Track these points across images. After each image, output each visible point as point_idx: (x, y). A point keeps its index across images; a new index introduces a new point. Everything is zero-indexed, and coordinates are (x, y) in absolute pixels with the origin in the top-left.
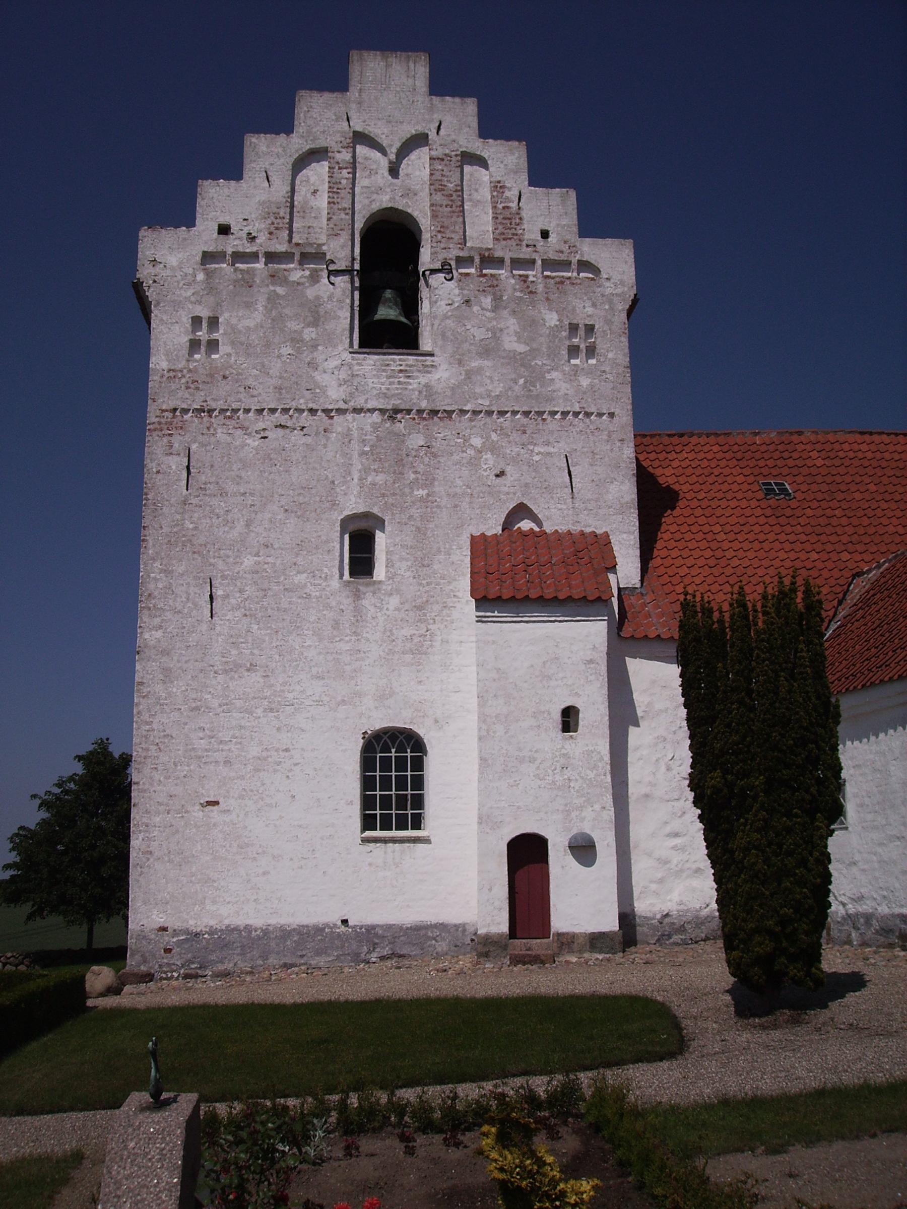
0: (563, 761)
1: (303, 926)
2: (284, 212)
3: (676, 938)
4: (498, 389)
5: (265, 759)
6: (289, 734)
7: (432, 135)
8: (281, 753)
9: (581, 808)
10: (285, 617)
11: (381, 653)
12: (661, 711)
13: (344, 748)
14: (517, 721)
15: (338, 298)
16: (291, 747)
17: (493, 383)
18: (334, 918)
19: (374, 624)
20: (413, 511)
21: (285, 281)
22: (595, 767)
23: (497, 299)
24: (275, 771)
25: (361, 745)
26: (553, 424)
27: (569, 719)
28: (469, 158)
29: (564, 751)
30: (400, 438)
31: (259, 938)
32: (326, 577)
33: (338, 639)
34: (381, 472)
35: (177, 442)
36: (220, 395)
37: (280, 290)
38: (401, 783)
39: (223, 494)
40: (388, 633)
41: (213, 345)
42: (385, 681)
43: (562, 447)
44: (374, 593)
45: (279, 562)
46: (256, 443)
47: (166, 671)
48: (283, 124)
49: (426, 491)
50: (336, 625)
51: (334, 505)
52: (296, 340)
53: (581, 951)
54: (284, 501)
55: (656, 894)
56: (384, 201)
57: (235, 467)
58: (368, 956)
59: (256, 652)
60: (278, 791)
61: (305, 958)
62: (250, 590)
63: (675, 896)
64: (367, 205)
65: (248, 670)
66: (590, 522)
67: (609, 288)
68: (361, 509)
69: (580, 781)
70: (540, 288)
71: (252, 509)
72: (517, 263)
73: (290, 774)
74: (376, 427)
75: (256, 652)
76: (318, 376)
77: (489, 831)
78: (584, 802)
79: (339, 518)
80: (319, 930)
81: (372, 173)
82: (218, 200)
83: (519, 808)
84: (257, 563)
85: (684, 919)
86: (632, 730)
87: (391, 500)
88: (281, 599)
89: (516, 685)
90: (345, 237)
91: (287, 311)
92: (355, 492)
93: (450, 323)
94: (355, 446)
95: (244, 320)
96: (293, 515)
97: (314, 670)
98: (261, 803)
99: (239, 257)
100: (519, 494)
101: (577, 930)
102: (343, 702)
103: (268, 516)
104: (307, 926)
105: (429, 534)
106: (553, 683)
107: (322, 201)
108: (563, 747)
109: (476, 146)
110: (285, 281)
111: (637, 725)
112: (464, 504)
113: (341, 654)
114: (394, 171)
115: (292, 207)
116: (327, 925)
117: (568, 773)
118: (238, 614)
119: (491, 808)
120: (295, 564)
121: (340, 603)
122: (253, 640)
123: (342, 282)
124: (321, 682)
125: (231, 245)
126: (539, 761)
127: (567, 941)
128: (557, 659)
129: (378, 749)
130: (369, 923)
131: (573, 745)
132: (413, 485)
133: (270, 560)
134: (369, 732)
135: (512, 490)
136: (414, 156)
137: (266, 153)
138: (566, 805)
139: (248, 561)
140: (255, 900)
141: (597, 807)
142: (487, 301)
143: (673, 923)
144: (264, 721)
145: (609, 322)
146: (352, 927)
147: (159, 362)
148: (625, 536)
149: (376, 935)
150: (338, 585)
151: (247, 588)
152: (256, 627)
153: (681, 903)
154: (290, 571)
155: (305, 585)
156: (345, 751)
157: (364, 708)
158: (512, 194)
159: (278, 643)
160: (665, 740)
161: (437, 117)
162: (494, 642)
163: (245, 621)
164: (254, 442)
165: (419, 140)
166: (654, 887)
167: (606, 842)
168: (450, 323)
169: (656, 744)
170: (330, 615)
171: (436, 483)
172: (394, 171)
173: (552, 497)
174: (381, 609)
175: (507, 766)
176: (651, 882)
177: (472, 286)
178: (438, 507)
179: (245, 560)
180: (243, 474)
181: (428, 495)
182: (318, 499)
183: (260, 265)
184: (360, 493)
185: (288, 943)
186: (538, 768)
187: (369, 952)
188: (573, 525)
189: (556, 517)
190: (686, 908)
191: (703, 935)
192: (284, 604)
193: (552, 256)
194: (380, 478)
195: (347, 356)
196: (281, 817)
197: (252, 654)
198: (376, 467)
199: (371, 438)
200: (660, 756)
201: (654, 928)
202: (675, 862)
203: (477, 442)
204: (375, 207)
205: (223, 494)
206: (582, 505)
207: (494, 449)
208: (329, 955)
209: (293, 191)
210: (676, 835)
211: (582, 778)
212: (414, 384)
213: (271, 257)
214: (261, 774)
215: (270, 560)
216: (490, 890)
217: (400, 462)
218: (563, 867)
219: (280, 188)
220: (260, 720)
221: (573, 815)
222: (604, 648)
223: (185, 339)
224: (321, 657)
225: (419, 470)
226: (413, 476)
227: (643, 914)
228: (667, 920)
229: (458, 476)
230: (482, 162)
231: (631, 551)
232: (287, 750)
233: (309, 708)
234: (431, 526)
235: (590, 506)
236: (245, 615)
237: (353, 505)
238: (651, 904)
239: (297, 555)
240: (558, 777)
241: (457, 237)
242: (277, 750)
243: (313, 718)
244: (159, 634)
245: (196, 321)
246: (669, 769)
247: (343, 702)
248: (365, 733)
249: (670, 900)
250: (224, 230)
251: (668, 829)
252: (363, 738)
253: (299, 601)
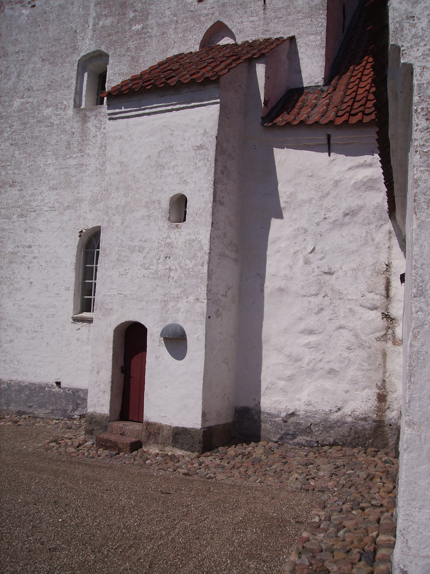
0: (167, 250)
1: (32, 384)
3: (300, 439)
5: (16, 253)
6: (32, 234)
8: (26, 249)
9: (177, 299)
10: (36, 143)
11: (98, 165)
12: (305, 202)
13: (66, 244)
14: (132, 211)
16: (32, 244)
18: (52, 380)
19: (94, 141)
22: (194, 257)
24: (22, 263)
25: (78, 242)
27: (179, 206)
29: (169, 241)
31: (6, 390)
32: (65, 108)
33: (68, 156)
34: (109, 16)
40: (104, 148)
42: (98, 188)
44: (96, 116)
45: (35, 101)
46: (28, 11)
49: (142, 25)
50: (69, 146)
51: (74, 49)
53: (164, 444)
54: (42, 52)
55: (284, 391)
57: (14, 33)
58: (73, 413)
59: (16, 171)
60: (22, 278)
61: (32, 409)
62: (16, 125)
63: (304, 396)
65: (10, 186)
66: (279, 29)
68: (93, 48)
69: (179, 271)
71: (23, 62)
73: (30, 266)
75: (16, 171)
77: (101, 317)
78: (181, 292)
79: (77, 60)
80: (41, 388)
83: (125, 296)
84: (22, 103)
85: (312, 421)
86: (275, 222)
87: (114, 38)
88: (35, 128)
89: (134, 177)
92: (89, 36)
96: (47, 62)
97: (52, 182)
98: (12, 287)
100: (217, 14)
101: (165, 422)
102: (68, 207)
103: (31, 66)
104: (34, 384)
105: (141, 60)
106: (165, 172)
108: (168, 237)
111: (280, 216)
112: (171, 30)
113: (70, 168)
116: (47, 385)
117: (170, 263)
118: (8, 144)
119: (105, 295)
120: (45, 100)
121: (72, 127)
122: (15, 163)
124: (55, 192)
126: (146, 250)
127: (154, 431)
128: (171, 147)
129: (96, 248)
130: (74, 387)
131: (177, 234)
132: (134, 20)
133: (30, 100)
134: (84, 231)
135: (211, 11)
138: (165, 295)
139: (17, 103)
140: (4, 361)
141: (191, 298)
143: (299, 424)
144: (17, 224)
146: (64, 389)
148: (312, 37)
149: (79, 396)
150: (72, 113)
151: (14, 124)
152: (17, 152)
153: (309, 404)
154: (42, 107)
155: (51, 116)
156: (67, 247)
157: (82, 211)
159: (30, 164)
160: (306, 231)
162: (121, 137)
163: (12, 148)
166: (282, 384)
167: (196, 336)
169: (296, 237)
170: (64, 137)
171: (150, 17)
173: (246, 12)
174: (100, 129)
175: (120, 256)
176: (279, 378)
178: (150, 37)
179: (15, 102)
180: (19, 37)
181: (143, 28)
182: (64, 46)
184: (92, 37)
185: (22, 396)
186: (145, 257)
187: (74, 410)
188: (263, 34)
190: (314, 410)
191: (331, 440)
192: (36, 134)
194: (108, 21)
196: (23, 299)
197: (14, 173)
198: (106, 13)
200: (298, 248)
201: (277, 425)
202: (306, 360)
206: (273, 15)
208: (47, 409)
210: (311, 332)
211: (181, 267)
214: (13, 265)
215: (30, 100)
216: (98, 372)
218: (157, 357)
220: (15, 224)
221: (171, 304)
222: (214, 132)
224: (57, 172)
225: (138, 8)
226: (132, 15)
227: (267, 410)
228: (292, 419)
229: (167, 7)
231: (317, 52)
232: (30, 247)
233: (46, 213)
234: (143, 54)
235: (280, 14)
236: (12, 145)
237: (87, 46)
238: (276, 402)
239: (47, 93)
240: (160, 267)
242: (24, 247)
243: (48, 221)
246: (307, 262)
247: (68, 207)
248: (81, 232)
249: (299, 400)
251: (302, 326)
252: (80, 236)
253: (46, 129)
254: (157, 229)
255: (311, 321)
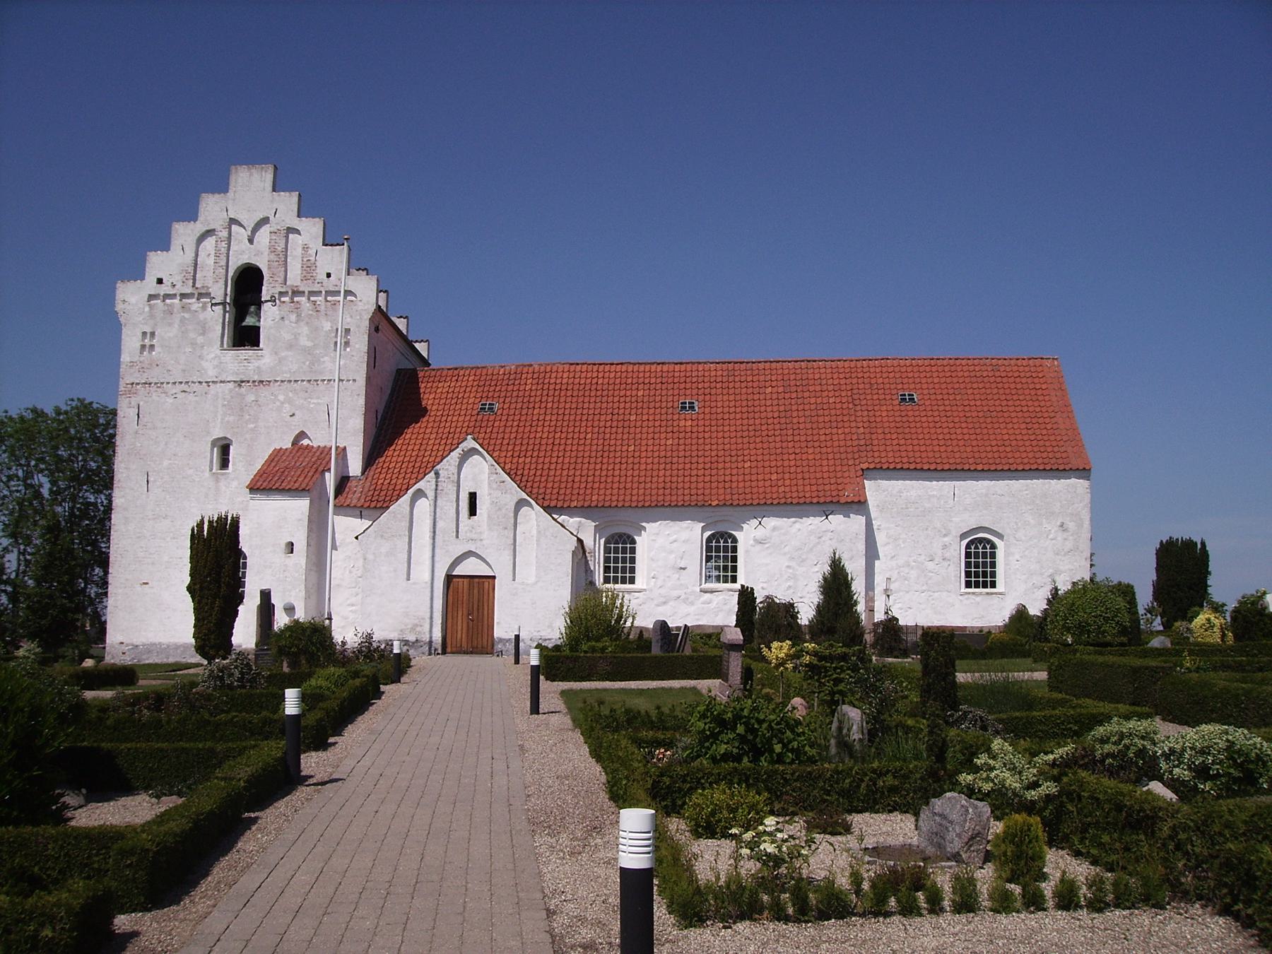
2: (191, 270)
4: (295, 367)
7: (272, 218)
15: (216, 319)
17: (293, 365)
20: (248, 436)
21: (189, 310)
23: (299, 316)
26: (322, 386)
27: (290, 547)
28: (292, 230)
30: (242, 396)
35: (134, 401)
36: (154, 375)
37: (186, 315)
38: (726, 558)
39: (155, 428)
41: (152, 347)
43: (325, 400)
47: (126, 518)
48: (192, 216)
50: (206, 496)
52: (193, 344)
56: (245, 259)
64: (236, 262)
67: (361, 306)
70: (323, 308)
72: (312, 293)
74: (231, 391)
76: (204, 364)
81: (240, 242)
82: (157, 263)
90: (222, 282)
91: (190, 327)
93: (272, 331)
94: (220, 401)
95: (167, 333)
99: (167, 296)
107: (211, 261)
109: (296, 223)
110: (189, 310)
114: (251, 241)
115: (196, 264)
123: (219, 309)
125: (163, 289)
136: (262, 230)
137: (184, 233)
139: (166, 463)
142: (293, 317)
145: (358, 327)
147: (125, 358)
158: (312, 252)
161: (275, 206)
164: (170, 400)
165: (265, 221)
168: (272, 331)
172: (251, 241)
177: (286, 308)
183: (176, 301)
189: (318, 438)
193: (332, 289)
194: (232, 418)
195: (218, 352)
199: (228, 397)
203: (281, 398)
204: (240, 263)
205: (155, 428)
207: (290, 401)
209: (197, 255)
212: (251, 366)
213: (183, 296)
217: (242, 409)
219: (190, 254)
223: (138, 345)
230: (297, 232)
237: (218, 433)
241: (281, 280)
244: (122, 500)
245: (144, 333)
250: (160, 281)
254: (280, 557)
255: (353, 600)
